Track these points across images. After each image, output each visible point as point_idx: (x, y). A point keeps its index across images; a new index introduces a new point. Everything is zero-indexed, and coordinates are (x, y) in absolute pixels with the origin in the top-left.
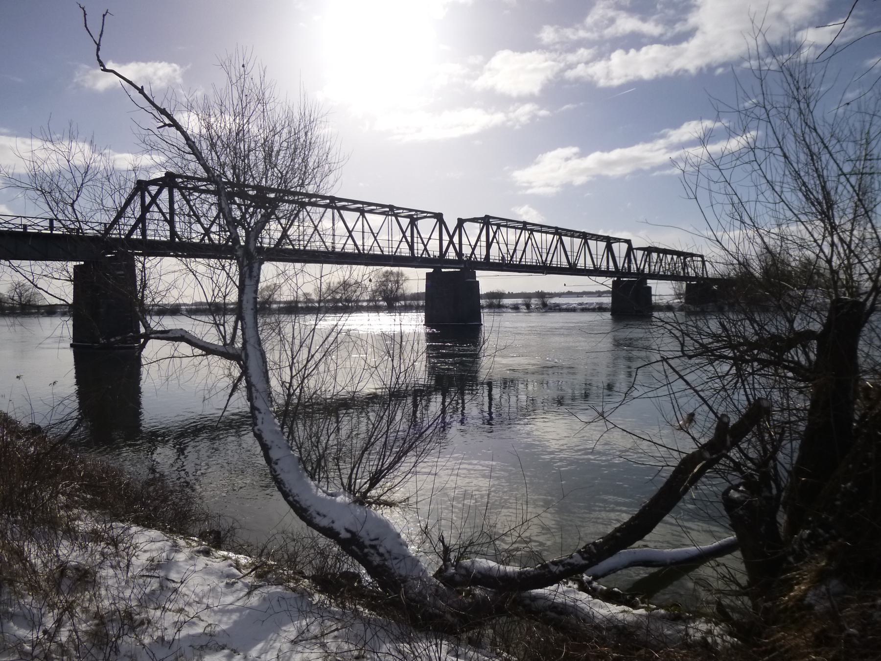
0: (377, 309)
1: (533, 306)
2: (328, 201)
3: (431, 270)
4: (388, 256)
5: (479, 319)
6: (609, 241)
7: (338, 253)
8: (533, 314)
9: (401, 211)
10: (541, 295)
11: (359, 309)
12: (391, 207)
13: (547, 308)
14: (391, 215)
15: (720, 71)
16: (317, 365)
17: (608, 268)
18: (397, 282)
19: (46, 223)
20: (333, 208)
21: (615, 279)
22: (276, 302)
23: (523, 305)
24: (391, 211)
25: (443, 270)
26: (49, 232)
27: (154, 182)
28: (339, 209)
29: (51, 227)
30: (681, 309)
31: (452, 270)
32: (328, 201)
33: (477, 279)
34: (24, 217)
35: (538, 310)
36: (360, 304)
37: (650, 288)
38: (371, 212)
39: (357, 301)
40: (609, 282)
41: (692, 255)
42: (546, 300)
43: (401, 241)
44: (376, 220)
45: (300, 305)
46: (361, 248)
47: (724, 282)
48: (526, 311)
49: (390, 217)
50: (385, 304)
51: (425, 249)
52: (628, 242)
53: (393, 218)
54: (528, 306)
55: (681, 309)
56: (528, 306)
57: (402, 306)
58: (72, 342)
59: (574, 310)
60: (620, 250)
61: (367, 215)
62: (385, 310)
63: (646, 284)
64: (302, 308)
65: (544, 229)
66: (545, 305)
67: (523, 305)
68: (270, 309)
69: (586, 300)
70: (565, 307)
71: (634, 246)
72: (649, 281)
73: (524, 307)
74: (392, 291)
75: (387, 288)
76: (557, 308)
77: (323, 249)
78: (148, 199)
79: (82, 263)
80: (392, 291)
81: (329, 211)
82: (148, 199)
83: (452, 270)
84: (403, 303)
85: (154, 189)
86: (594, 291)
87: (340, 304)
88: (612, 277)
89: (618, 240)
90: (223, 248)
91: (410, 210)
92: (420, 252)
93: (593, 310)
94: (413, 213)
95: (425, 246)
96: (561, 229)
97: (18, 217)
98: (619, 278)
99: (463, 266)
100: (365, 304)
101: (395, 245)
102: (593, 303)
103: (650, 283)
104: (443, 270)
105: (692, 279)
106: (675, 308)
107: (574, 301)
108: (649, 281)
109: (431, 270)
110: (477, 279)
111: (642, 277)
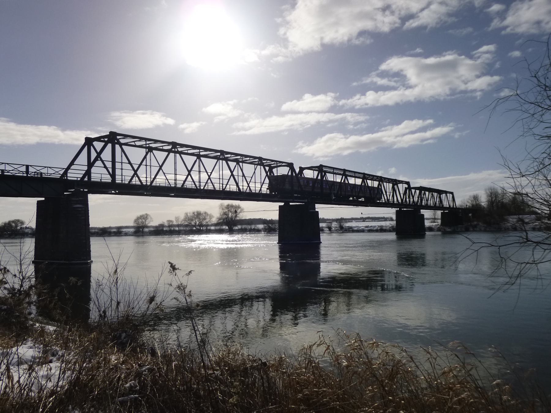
0: (221, 232)
1: (333, 229)
2: (219, 154)
3: (282, 204)
4: (255, 193)
5: (319, 239)
6: (395, 182)
7: (179, 188)
8: (334, 234)
9: (248, 159)
10: (340, 221)
11: (208, 232)
12: (222, 152)
13: (344, 230)
14: (222, 159)
15: (419, 50)
16: (113, 281)
17: (394, 201)
18: (236, 212)
19: (24, 169)
20: (175, 152)
21: (398, 209)
22: (147, 227)
23: (327, 227)
24: (260, 161)
25: (291, 204)
26: (26, 175)
27: (98, 139)
28: (181, 153)
29: (27, 171)
30: (439, 230)
31: (298, 204)
32: (219, 154)
33: (316, 210)
34: (7, 164)
35: (337, 231)
36: (209, 228)
37: (423, 215)
38: (206, 156)
39: (207, 226)
40: (394, 210)
41: (446, 192)
42: (342, 224)
43: (250, 182)
44: (248, 169)
45: (165, 229)
46: (197, 184)
47: (464, 211)
48: (329, 232)
49: (221, 161)
50: (227, 228)
51: (249, 186)
52: (408, 183)
53: (224, 162)
54: (330, 228)
55: (439, 230)
56: (330, 228)
57: (239, 229)
58: (33, 259)
59: (363, 231)
60: (402, 187)
61: (202, 158)
62: (227, 232)
63: (420, 212)
64: (166, 231)
65: (336, 171)
66: (341, 228)
67: (327, 227)
68: (143, 232)
69: (383, 223)
70: (356, 229)
71: (412, 186)
72: (422, 211)
73: (327, 229)
74: (232, 218)
75: (228, 217)
76: (351, 230)
77: (194, 187)
78: (94, 155)
79: (43, 199)
80: (232, 218)
81: (259, 167)
82: (94, 155)
83: (298, 204)
84: (239, 227)
85: (98, 145)
86: (359, 217)
87: (194, 228)
88: (395, 208)
89: (401, 182)
90: (202, 191)
91: (146, 139)
92: (245, 188)
93: (377, 231)
94: (239, 157)
95: (248, 184)
96: (265, 159)
97: (3, 163)
98: (400, 209)
99: (306, 201)
100: (213, 228)
101: (225, 182)
102: (376, 226)
103: (423, 211)
104: (291, 204)
105: (446, 208)
106: (434, 229)
107: (362, 225)
108: (422, 211)
109: (282, 204)
110: (316, 210)
111: (417, 207)
